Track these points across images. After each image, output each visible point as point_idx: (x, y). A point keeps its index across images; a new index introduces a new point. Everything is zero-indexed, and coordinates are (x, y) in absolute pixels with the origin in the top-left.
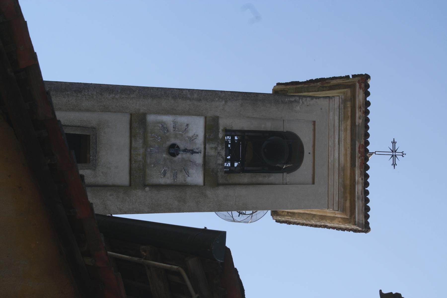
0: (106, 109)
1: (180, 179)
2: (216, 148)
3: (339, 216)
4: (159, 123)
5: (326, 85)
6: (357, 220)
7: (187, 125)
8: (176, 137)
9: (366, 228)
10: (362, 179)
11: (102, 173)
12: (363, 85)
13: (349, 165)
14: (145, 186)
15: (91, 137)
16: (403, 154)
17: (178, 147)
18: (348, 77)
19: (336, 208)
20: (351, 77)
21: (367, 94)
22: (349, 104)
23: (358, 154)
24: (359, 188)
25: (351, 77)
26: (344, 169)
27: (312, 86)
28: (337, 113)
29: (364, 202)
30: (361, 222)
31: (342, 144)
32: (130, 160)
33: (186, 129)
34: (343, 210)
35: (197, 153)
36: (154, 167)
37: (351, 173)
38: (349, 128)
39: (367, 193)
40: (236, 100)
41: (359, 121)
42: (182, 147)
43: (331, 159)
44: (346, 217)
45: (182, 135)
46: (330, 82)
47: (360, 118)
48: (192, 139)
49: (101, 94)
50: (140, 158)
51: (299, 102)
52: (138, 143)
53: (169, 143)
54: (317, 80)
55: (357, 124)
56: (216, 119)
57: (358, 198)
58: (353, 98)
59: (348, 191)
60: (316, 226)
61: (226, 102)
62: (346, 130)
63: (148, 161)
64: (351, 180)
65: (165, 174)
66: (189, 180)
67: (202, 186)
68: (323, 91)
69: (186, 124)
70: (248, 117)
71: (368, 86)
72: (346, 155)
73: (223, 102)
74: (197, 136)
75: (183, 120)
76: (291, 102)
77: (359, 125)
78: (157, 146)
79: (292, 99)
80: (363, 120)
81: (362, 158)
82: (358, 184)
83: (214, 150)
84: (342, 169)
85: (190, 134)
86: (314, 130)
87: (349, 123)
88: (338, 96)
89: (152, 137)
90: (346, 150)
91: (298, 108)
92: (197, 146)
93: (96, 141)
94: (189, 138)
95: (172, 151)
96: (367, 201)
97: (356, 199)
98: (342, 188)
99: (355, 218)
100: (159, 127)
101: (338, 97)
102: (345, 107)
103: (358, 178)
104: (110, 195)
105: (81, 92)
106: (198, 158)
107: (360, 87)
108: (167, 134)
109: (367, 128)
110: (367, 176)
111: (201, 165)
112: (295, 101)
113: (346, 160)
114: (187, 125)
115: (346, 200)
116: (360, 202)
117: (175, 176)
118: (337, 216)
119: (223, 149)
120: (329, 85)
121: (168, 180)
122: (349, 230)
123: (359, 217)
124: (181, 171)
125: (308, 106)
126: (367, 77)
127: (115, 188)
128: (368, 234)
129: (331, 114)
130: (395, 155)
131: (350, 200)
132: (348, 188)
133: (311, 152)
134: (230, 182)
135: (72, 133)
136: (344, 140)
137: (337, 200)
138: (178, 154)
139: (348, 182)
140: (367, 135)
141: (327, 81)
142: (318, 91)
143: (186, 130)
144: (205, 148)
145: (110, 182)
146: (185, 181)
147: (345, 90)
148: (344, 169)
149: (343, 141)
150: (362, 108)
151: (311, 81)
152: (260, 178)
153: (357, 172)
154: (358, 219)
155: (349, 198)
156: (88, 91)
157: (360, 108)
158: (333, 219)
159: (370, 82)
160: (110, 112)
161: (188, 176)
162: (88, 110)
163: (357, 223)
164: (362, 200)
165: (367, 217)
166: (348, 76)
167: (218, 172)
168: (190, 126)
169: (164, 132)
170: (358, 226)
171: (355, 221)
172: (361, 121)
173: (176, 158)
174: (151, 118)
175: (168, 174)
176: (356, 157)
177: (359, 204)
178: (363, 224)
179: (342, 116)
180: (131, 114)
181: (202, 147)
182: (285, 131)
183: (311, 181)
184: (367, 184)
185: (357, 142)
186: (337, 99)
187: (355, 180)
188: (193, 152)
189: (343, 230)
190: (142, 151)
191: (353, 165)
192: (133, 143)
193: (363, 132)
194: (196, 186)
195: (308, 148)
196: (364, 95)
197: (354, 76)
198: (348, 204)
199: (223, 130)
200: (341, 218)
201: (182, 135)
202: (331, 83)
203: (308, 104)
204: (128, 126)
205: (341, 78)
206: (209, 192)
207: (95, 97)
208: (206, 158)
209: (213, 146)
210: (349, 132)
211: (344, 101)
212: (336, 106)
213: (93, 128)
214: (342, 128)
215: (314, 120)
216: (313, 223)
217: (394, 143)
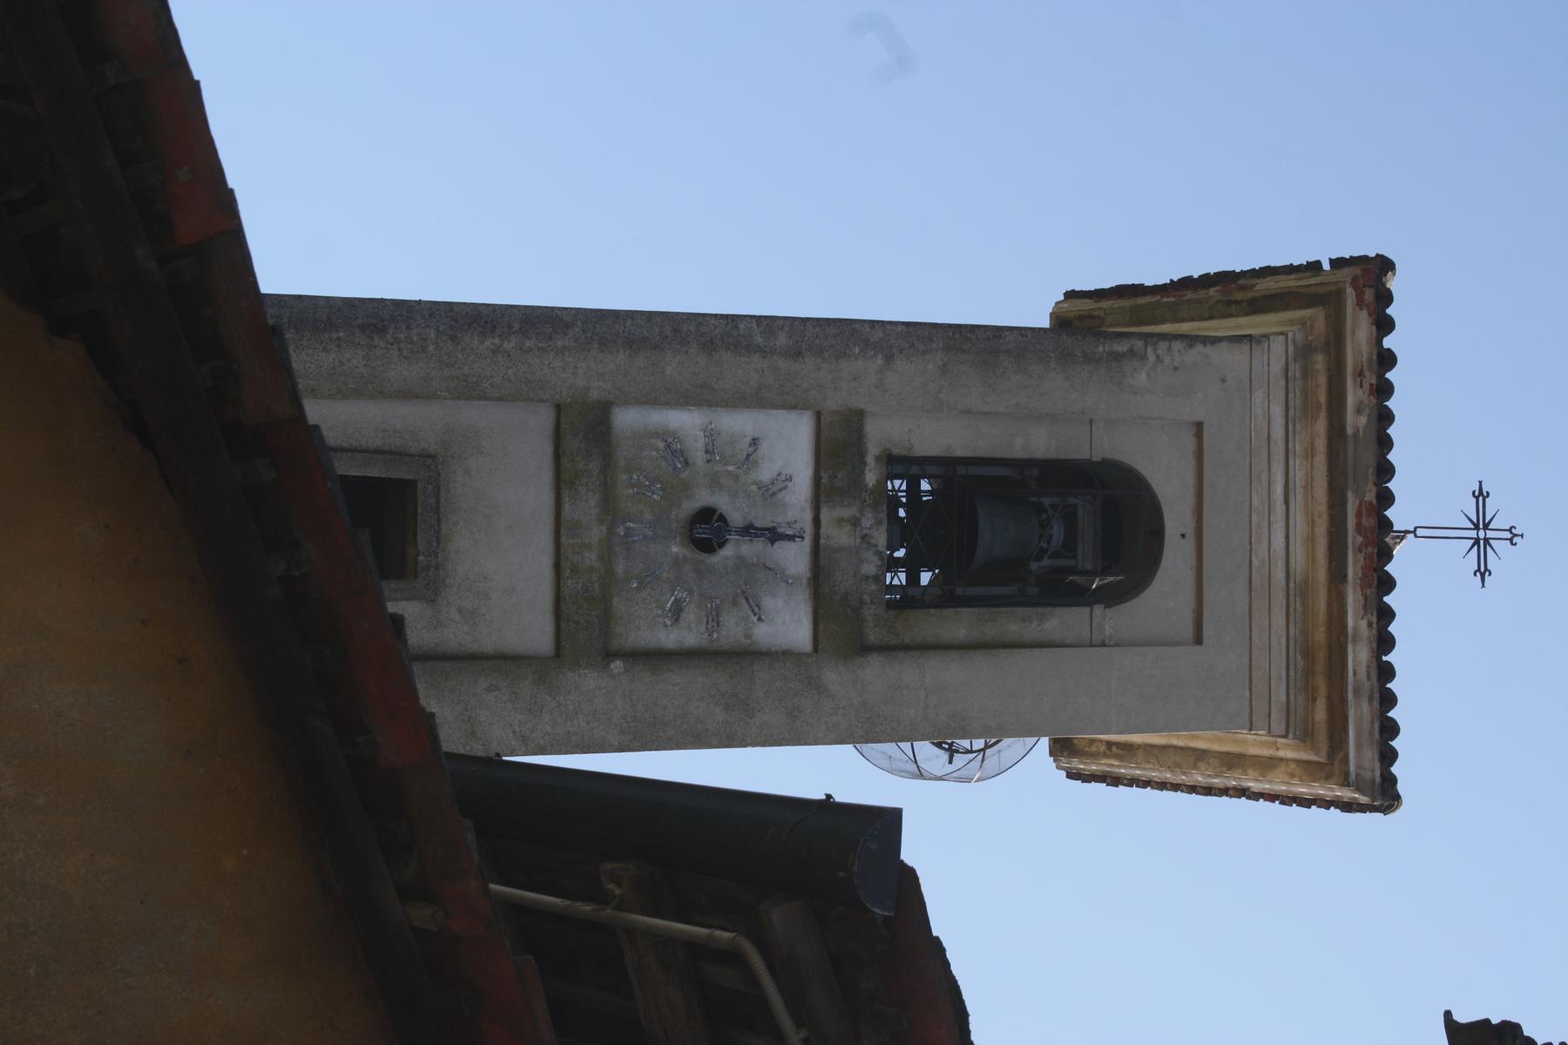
0: (470, 391)
1: (731, 630)
2: (855, 522)
3: (1290, 754)
4: (655, 434)
5: (1239, 296)
6: (1352, 768)
7: (755, 442)
8: (715, 483)
9: (1385, 797)
10: (1370, 625)
11: (460, 610)
12: (1369, 294)
13: (1322, 574)
14: (610, 655)
15: (420, 486)
16: (1513, 536)
17: (722, 518)
18: (1315, 266)
19: (1279, 727)
20: (1326, 266)
22: (1320, 362)
23: (1353, 538)
24: (1359, 656)
25: (1326, 266)
27: (1189, 301)
29: (1376, 704)
30: (1368, 775)
31: (1298, 502)
32: (557, 566)
33: (748, 456)
34: (1306, 736)
35: (791, 538)
37: (1329, 605)
38: (1321, 444)
39: (1387, 672)
40: (924, 353)
41: (1356, 422)
42: (736, 518)
44: (1314, 758)
45: (736, 477)
46: (1254, 286)
47: (1358, 411)
49: (453, 338)
50: (591, 558)
51: (1143, 357)
52: (584, 507)
53: (689, 507)
54: (1207, 280)
55: (1350, 431)
56: (854, 421)
57: (1357, 692)
58: (1335, 341)
59: (1320, 666)
61: (889, 358)
62: (1310, 453)
63: (620, 568)
64: (1329, 627)
65: (677, 612)
66: (764, 634)
68: (1230, 316)
69: (749, 439)
70: (969, 412)
71: (1386, 298)
72: (1310, 540)
73: (880, 361)
74: (790, 479)
75: (739, 423)
76: (1118, 357)
77: (1356, 435)
78: (648, 516)
79: (1121, 347)
81: (1370, 549)
82: (1355, 641)
83: (847, 528)
84: (1299, 591)
85: (765, 473)
86: (1199, 454)
87: (1321, 426)
88: (1282, 334)
89: (633, 486)
90: (1312, 524)
91: (1141, 378)
92: (790, 515)
93: (438, 501)
94: (760, 485)
95: (702, 532)
96: (1389, 700)
97: (1350, 696)
98: (1299, 658)
99: (1346, 760)
101: (1281, 338)
102: (1306, 374)
103: (1356, 621)
104: (489, 690)
105: (382, 331)
106: (795, 558)
107: (1360, 303)
109: (1386, 443)
110: (1387, 614)
111: (805, 581)
112: (1131, 353)
113: (1311, 557)
114: (755, 442)
115: (1314, 700)
116: (1365, 706)
118: (1281, 754)
119: (878, 523)
120: (1249, 295)
121: (688, 635)
122: (1326, 804)
123: (1360, 757)
124: (735, 603)
125: (1176, 369)
126: (1384, 265)
129: (1259, 396)
131: (1329, 698)
132: (1321, 655)
133: (1190, 532)
134: (907, 640)
136: (1305, 487)
138: (721, 545)
139: (1320, 635)
140: (1386, 471)
141: (1242, 282)
142: (1211, 318)
143: (750, 461)
144: (817, 521)
146: (748, 636)
149: (1299, 490)
150: (1367, 374)
151: (1186, 283)
152: (1012, 623)
154: (1359, 767)
155: (1322, 692)
157: (1361, 374)
159: (1394, 284)
161: (760, 619)
162: (407, 394)
163: (1352, 778)
164: (1371, 699)
165: (1389, 756)
168: (764, 447)
169: (675, 468)
170: (1358, 790)
171: (1347, 774)
172: (1363, 420)
173: (715, 559)
174: (627, 419)
175: (690, 614)
177: (1359, 713)
180: (558, 407)
181: (807, 517)
182: (1096, 458)
183: (1188, 631)
184: (1386, 642)
185: (1350, 496)
186: (1278, 346)
187: (1345, 626)
188: (774, 535)
189: (1305, 802)
190: (596, 533)
191: (1337, 574)
192: (567, 507)
193: (1369, 459)
194: (786, 654)
195: (1176, 519)
197: (1337, 263)
198: (1320, 714)
199: (878, 459)
200: (1297, 761)
201: (736, 477)
202: (1257, 288)
204: (549, 450)
205: (1290, 269)
206: (834, 676)
207: (431, 348)
208: (822, 555)
209: (846, 513)
211: (1305, 352)
212: (1277, 367)
213: (427, 457)
214: (1298, 447)
215: (1199, 417)
217: (1480, 495)
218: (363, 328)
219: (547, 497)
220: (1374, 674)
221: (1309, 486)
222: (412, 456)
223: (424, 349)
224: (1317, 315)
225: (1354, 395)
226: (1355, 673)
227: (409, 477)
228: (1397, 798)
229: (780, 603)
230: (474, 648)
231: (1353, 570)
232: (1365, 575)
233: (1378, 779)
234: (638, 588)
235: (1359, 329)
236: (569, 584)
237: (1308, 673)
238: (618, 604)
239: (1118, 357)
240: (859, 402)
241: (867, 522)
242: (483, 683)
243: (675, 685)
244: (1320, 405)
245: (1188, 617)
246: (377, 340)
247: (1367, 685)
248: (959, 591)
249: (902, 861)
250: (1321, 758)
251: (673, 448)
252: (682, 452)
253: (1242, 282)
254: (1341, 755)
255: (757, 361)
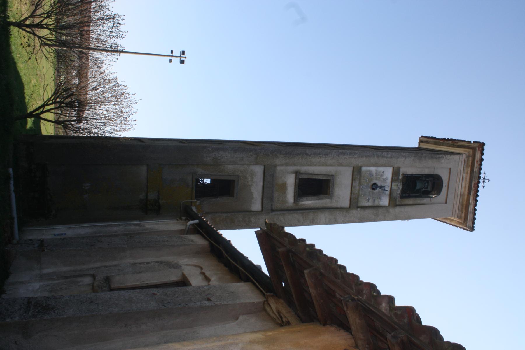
0: (340, 165)
1: (376, 203)
2: (397, 185)
3: (456, 220)
4: (368, 171)
5: (456, 144)
6: (468, 225)
7: (383, 172)
8: (376, 179)
9: (472, 229)
10: (474, 202)
11: (335, 200)
12: (481, 149)
13: (466, 193)
14: (358, 207)
15: (331, 180)
17: (377, 185)
18: (470, 142)
19: (456, 216)
20: (472, 142)
21: (482, 154)
22: (470, 159)
23: (473, 188)
24: (471, 207)
25: (472, 142)
26: (463, 195)
27: (446, 143)
28: (463, 163)
29: (473, 215)
30: (470, 226)
31: (464, 181)
33: (382, 175)
34: (460, 218)
36: (363, 196)
37: (467, 198)
38: (469, 172)
39: (475, 210)
40: (411, 157)
41: (476, 169)
42: (379, 185)
43: (457, 189)
44: (461, 222)
45: (380, 178)
46: (458, 143)
47: (476, 168)
48: (385, 180)
49: (339, 156)
50: (356, 192)
51: (444, 158)
52: (356, 184)
53: (372, 183)
54: (448, 140)
55: (474, 171)
56: (399, 169)
57: (470, 213)
59: (464, 207)
60: (439, 221)
61: (405, 158)
62: (467, 173)
63: (361, 193)
64: (467, 202)
67: (387, 207)
68: (454, 147)
69: (382, 172)
70: (416, 167)
71: (483, 150)
72: (465, 187)
73: (404, 159)
74: (388, 178)
75: (381, 169)
76: (440, 157)
77: (475, 172)
78: (366, 184)
79: (441, 156)
80: (478, 169)
81: (475, 190)
82: (471, 204)
83: (396, 186)
84: (462, 195)
85: (384, 177)
86: (450, 173)
87: (469, 169)
88: (465, 153)
89: (364, 180)
90: (466, 185)
91: (443, 161)
92: (387, 184)
93: (334, 183)
94: (383, 179)
95: (374, 187)
96: (475, 214)
97: (469, 213)
98: (461, 206)
99: (467, 223)
100: (368, 173)
101: (465, 154)
102: (468, 160)
103: (472, 201)
104: (339, 213)
105: (327, 155)
107: (479, 150)
108: (372, 178)
110: (477, 201)
111: (388, 195)
112: (442, 157)
113: (465, 190)
115: (462, 213)
116: (471, 215)
117: (374, 201)
118: (455, 219)
119: (400, 185)
120: (457, 144)
122: (461, 228)
123: (469, 223)
124: (377, 198)
125: (448, 159)
126: (484, 144)
127: (341, 209)
128: (472, 232)
129: (460, 163)
130: (485, 181)
131: (465, 213)
132: (465, 206)
133: (447, 186)
134: (403, 204)
135: (321, 178)
136: (465, 179)
137: (457, 212)
138: (376, 189)
139: (465, 203)
141: (456, 141)
142: (450, 147)
143: (382, 175)
144: (391, 185)
145: (339, 206)
146: (379, 204)
147: (469, 150)
148: (463, 195)
149: (464, 179)
150: (479, 162)
151: (444, 139)
152: (419, 201)
153: (471, 198)
154: (469, 224)
155: (464, 211)
156: (332, 154)
157: (478, 162)
158: (452, 220)
159: (485, 147)
160: (343, 166)
161: (381, 201)
162: (331, 165)
163: (467, 226)
164: (472, 214)
165: (474, 223)
166: (470, 142)
167: (397, 198)
168: (385, 173)
169: (371, 177)
170: (468, 228)
172: (477, 169)
174: (364, 169)
175: (370, 200)
176: (471, 189)
177: (470, 216)
178: (471, 227)
179: (466, 165)
180: (354, 167)
181: (390, 184)
182: (435, 174)
183: (444, 202)
184: (476, 205)
186: (464, 155)
187: (470, 202)
189: (457, 227)
190: (357, 188)
192: (353, 184)
193: (477, 175)
194: (384, 207)
195: (445, 183)
196: (481, 154)
197: (475, 142)
198: (463, 215)
199: (402, 175)
200: (458, 221)
201: (380, 178)
202: (459, 143)
203: (449, 158)
204: (351, 174)
205: (465, 141)
206: (391, 210)
207: (335, 158)
208: (392, 190)
209: (396, 184)
210: (469, 175)
211: (468, 157)
212: (463, 159)
213: (333, 175)
214: (465, 172)
215: (451, 167)
216: (438, 219)
218: (325, 155)
219: (350, 182)
220: (473, 210)
221: (466, 179)
222: (330, 175)
223: (334, 158)
224: (471, 151)
225: (476, 165)
226: (470, 210)
227: (330, 179)
228: (474, 230)
229: (384, 198)
230: (337, 207)
231: (472, 192)
232: (474, 194)
233: (471, 227)
234: (363, 196)
235: (478, 154)
236: (353, 196)
237: (462, 209)
238: (360, 199)
239: (440, 157)
240: (400, 166)
241: (399, 185)
242: (338, 212)
243: (368, 212)
244: (469, 166)
245: (445, 199)
246: (327, 157)
247: (472, 212)
248: (411, 195)
249: (448, 343)
250: (462, 222)
251: (371, 174)
252: (372, 174)
253: (456, 141)
254: (466, 222)
255: (385, 159)
